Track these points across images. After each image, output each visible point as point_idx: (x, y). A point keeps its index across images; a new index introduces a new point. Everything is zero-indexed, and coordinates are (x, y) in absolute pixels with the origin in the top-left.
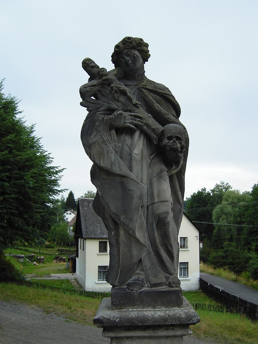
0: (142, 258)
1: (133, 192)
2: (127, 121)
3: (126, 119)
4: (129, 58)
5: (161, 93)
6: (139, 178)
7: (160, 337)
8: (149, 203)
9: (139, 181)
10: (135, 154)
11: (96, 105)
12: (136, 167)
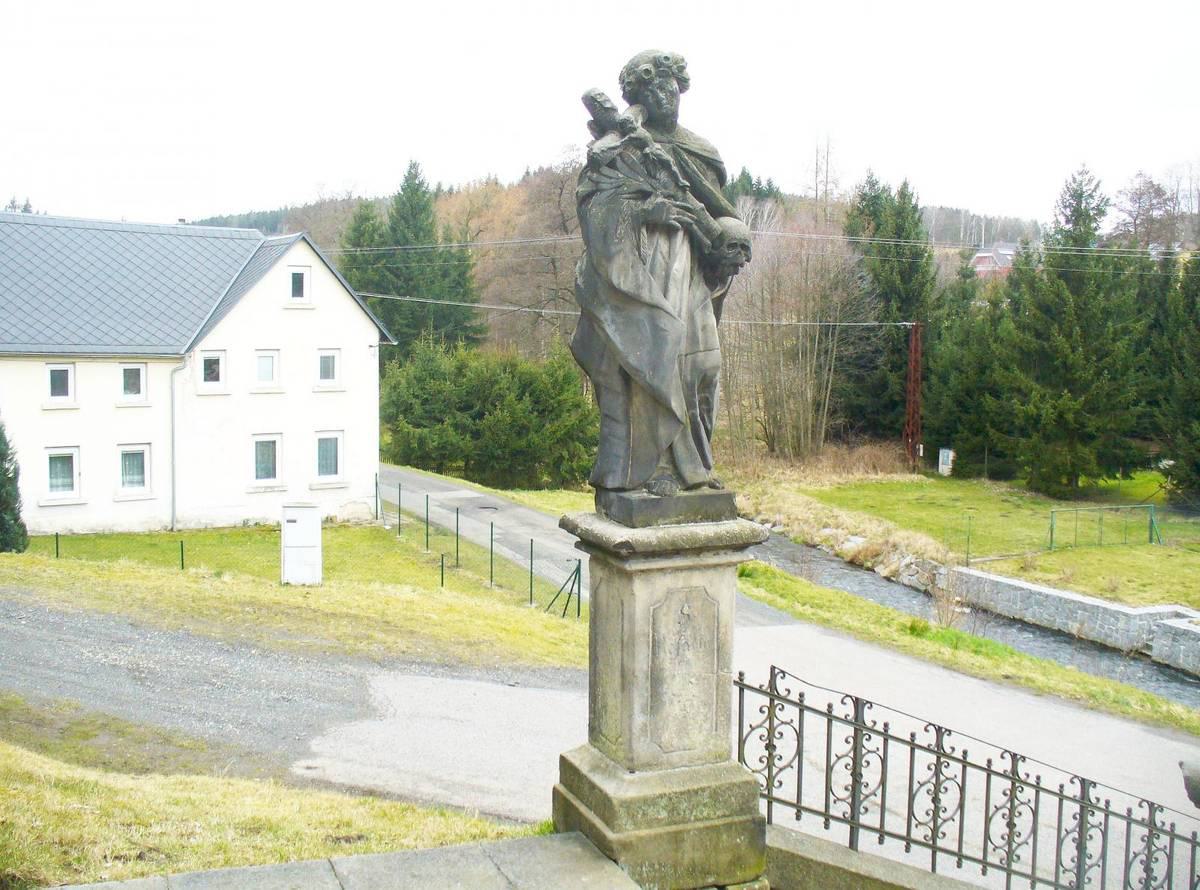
4: (1106, 420)
6: (677, 309)
7: (708, 567)
8: (688, 352)
11: (612, 180)
12: (673, 291)
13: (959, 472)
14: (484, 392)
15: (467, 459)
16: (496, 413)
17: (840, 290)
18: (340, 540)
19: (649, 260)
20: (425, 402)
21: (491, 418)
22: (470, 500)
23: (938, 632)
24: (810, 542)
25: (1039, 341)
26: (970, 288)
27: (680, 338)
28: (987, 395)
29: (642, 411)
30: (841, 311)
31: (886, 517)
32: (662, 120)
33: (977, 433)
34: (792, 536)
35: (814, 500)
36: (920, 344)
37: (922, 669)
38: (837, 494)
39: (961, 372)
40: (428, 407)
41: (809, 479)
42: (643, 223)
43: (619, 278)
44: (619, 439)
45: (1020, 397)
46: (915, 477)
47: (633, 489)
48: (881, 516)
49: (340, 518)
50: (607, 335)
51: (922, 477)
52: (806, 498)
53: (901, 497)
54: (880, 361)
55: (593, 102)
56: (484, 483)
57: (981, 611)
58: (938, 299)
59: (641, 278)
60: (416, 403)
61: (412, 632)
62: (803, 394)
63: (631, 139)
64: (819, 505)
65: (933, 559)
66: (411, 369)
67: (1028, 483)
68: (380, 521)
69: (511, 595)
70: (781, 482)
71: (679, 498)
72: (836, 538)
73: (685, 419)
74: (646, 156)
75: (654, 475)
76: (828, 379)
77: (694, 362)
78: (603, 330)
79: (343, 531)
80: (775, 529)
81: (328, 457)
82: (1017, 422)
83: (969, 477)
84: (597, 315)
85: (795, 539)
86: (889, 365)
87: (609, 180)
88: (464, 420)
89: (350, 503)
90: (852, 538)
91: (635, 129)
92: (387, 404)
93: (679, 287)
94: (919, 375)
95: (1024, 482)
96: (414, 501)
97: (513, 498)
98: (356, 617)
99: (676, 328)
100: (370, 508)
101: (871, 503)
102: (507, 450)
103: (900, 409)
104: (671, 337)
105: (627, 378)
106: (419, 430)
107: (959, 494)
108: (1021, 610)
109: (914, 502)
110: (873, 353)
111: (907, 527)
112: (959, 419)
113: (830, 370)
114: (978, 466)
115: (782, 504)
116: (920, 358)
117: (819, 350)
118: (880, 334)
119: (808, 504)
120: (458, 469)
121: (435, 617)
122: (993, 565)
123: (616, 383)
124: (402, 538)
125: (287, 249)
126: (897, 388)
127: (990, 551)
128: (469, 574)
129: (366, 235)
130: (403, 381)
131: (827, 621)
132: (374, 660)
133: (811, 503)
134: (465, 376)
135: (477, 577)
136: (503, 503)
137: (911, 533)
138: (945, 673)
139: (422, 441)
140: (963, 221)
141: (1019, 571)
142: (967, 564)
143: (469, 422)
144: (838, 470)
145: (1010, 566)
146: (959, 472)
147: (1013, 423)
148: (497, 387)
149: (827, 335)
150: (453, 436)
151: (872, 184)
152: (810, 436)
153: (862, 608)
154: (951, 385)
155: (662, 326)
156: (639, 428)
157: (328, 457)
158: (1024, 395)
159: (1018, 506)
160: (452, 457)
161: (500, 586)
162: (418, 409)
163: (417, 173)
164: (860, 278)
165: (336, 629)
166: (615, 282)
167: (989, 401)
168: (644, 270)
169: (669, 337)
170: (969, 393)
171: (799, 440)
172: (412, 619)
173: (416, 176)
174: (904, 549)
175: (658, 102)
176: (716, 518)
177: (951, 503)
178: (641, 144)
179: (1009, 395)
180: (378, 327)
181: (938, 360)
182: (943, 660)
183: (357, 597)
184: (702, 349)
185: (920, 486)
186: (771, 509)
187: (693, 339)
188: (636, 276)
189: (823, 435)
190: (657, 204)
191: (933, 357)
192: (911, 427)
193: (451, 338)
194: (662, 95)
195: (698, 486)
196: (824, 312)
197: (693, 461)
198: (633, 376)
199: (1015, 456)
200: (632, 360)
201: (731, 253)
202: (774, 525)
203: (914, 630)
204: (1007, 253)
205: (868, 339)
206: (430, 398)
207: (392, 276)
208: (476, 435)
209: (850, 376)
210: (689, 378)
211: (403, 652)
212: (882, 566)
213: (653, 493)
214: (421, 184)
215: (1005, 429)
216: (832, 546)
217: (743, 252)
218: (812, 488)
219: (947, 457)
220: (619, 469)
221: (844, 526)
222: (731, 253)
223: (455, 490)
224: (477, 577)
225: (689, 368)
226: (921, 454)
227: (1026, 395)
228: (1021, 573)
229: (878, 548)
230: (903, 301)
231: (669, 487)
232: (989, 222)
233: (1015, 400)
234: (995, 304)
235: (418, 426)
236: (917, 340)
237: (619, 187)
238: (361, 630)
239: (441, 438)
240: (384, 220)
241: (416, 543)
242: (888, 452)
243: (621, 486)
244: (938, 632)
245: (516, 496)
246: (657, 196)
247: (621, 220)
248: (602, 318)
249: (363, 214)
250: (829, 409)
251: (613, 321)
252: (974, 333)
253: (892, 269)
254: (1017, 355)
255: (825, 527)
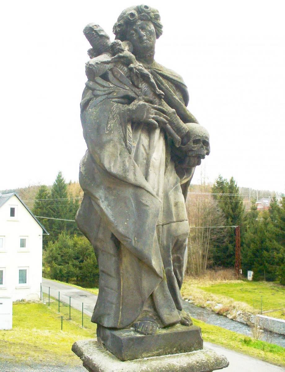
0: (155, 292)
1: (148, 208)
2: (151, 115)
3: (150, 113)
5: (173, 81)
6: (156, 190)
8: (165, 222)
9: (154, 194)
10: (154, 158)
11: (105, 89)
13: (255, 279)
14: (83, 253)
15: (77, 277)
16: (88, 260)
17: (210, 215)
18: (26, 308)
19: (133, 150)
20: (62, 256)
21: (86, 262)
22: (77, 293)
23: (255, 342)
24: (202, 306)
25: (282, 231)
26: (255, 214)
27: (158, 211)
28: (264, 251)
29: (129, 269)
30: (211, 222)
31: (230, 296)
32: (145, 53)
33: (261, 265)
34: (196, 304)
35: (203, 291)
36: (239, 233)
37: (254, 361)
38: (212, 288)
39: (255, 243)
40: (63, 258)
41: (201, 283)
42: (128, 121)
43: (110, 163)
44: (112, 289)
45: (276, 251)
46: (239, 281)
47: (123, 328)
48: (228, 296)
49: (27, 300)
50: (101, 210)
51: (242, 281)
52: (201, 290)
53: (235, 289)
54: (225, 240)
55: (92, 34)
56: (83, 286)
57: (268, 332)
58: (245, 218)
59: (127, 164)
60: (59, 257)
61: (46, 351)
62: (198, 252)
63: (120, 57)
64: (205, 293)
65: (249, 312)
66: (57, 244)
67: (280, 282)
68: (42, 301)
69: (90, 331)
70: (191, 285)
71: (158, 336)
72: (212, 305)
73: (163, 275)
74: (131, 70)
75: (140, 317)
76: (207, 247)
77: (169, 230)
78: (99, 206)
79: (28, 305)
80: (190, 302)
81: (23, 277)
82: (276, 260)
83: (259, 281)
84: (94, 194)
85: (197, 305)
86: (229, 241)
87: (102, 89)
88: (76, 263)
89: (31, 294)
90: (218, 305)
91: (123, 50)
92: (49, 257)
93: (157, 172)
94: (239, 244)
95: (279, 282)
96: (54, 293)
97: (93, 292)
98: (23, 344)
99: (155, 204)
100: (39, 296)
101: (224, 291)
102: (92, 274)
103: (233, 257)
104: (151, 211)
105: (117, 243)
106: (60, 266)
107: (256, 287)
108: (283, 331)
109: (240, 291)
110: (223, 237)
111: (238, 300)
112: (255, 260)
113: (207, 244)
114: (262, 277)
115: (191, 292)
116: (240, 239)
117: (204, 237)
118: (225, 230)
119: (201, 292)
120: (74, 281)
121: (56, 344)
122: (271, 314)
123: (110, 247)
124: (50, 308)
125: (8, 199)
126: (232, 249)
127: (270, 308)
128: (74, 322)
129: (43, 196)
130: (54, 249)
131: (213, 341)
132: (28, 365)
133: (202, 292)
134: (77, 247)
135: (77, 324)
136: (90, 294)
137: (240, 302)
138: (264, 363)
139: (61, 271)
140: (250, 191)
141: (281, 315)
142: (262, 314)
143: (78, 263)
144: (212, 279)
145: (278, 314)
146: (255, 279)
147: (274, 260)
148: (88, 251)
149: (206, 231)
150: (72, 269)
151: (221, 178)
152: (201, 267)
153: (224, 332)
154: (251, 248)
155: (144, 202)
156: (128, 281)
157: (23, 277)
158: (278, 251)
159: (278, 291)
160: (72, 276)
161: (86, 327)
162: (59, 258)
163: (61, 175)
164: (217, 211)
165: (14, 350)
166: (107, 165)
167: (265, 253)
168: (130, 158)
169: (150, 211)
170: (257, 250)
171: (197, 269)
172: (46, 345)
173: (61, 176)
174: (237, 308)
175: (140, 37)
176: (186, 348)
177: (253, 291)
178: (126, 62)
179: (272, 251)
180: (42, 228)
181: (246, 239)
182: (261, 357)
183: (25, 335)
184: (175, 220)
185: (241, 285)
186: (188, 294)
187: (168, 213)
188: (124, 162)
189: (206, 267)
190: (139, 105)
191: (244, 238)
192: (237, 263)
193: (72, 233)
194: (143, 33)
195: (172, 325)
196: (204, 223)
197: (169, 307)
198: (122, 242)
199: (275, 272)
200: (121, 229)
201: (196, 147)
202: (189, 300)
203: (246, 342)
204: (267, 202)
205: (221, 232)
206: (64, 254)
207: (52, 211)
208: (81, 268)
209: (215, 246)
210: (165, 243)
211: (41, 361)
212: (229, 315)
213: (138, 332)
214: (63, 179)
215: (271, 263)
216: (211, 307)
217: (204, 147)
218: (202, 286)
219: (250, 274)
220: (112, 313)
221: (215, 300)
222: (196, 147)
223: (72, 289)
224: (77, 324)
225: (165, 235)
226: (241, 273)
227: (278, 251)
228: (282, 317)
229: (228, 308)
230: (233, 218)
231: (151, 328)
232: (259, 192)
233: (274, 252)
234: (266, 219)
235: (60, 265)
236: (238, 232)
237: (110, 93)
238: (24, 351)
239: (68, 269)
240: (49, 192)
241: (54, 309)
242: (230, 272)
243: (113, 326)
244: (255, 342)
245: (93, 291)
246: (139, 100)
247: (111, 117)
248: (97, 195)
249: (42, 191)
250: (207, 258)
251: (106, 198)
252: (258, 229)
253: (229, 207)
254: (274, 236)
255: (208, 301)
